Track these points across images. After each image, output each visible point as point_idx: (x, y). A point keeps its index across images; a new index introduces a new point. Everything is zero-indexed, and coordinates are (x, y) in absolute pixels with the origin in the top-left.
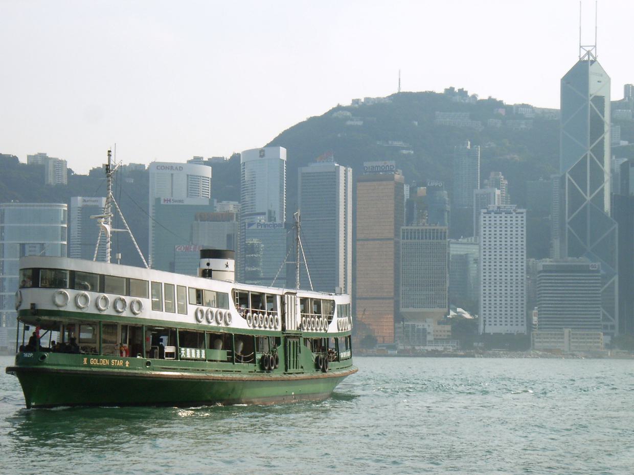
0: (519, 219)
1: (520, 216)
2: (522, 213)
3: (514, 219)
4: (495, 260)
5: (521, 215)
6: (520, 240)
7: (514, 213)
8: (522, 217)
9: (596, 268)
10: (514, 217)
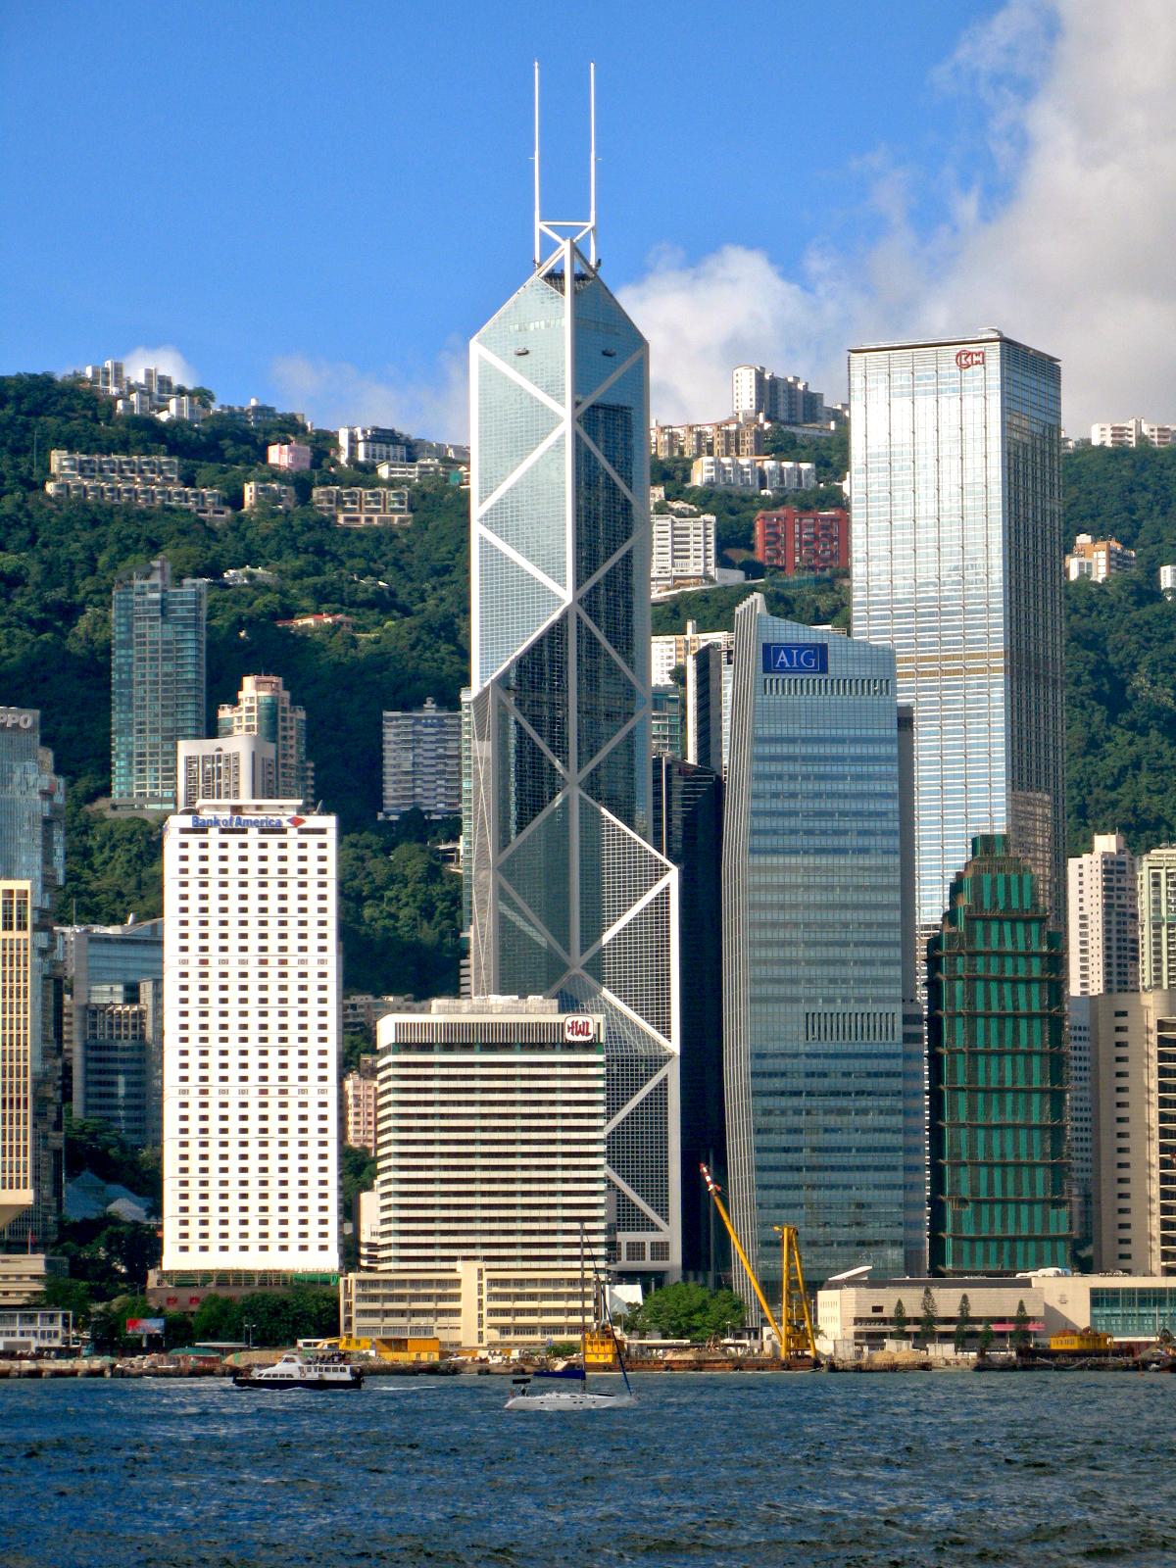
0: (312, 852)
1: (313, 840)
2: (322, 831)
3: (293, 852)
4: (283, 1007)
7: (293, 832)
8: (323, 846)
9: (588, 1034)
10: (293, 845)
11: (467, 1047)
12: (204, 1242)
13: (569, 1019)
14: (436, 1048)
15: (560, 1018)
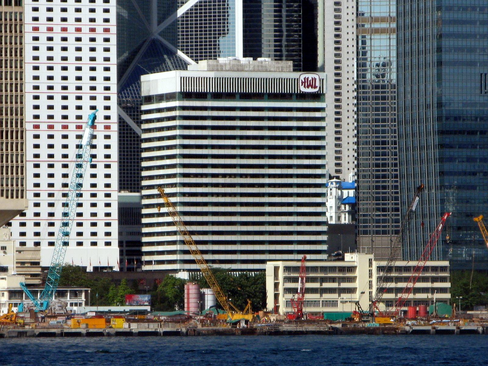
9: (315, 87)
11: (230, 96)
12: (94, 239)
13: (303, 76)
14: (209, 96)
15: (296, 75)
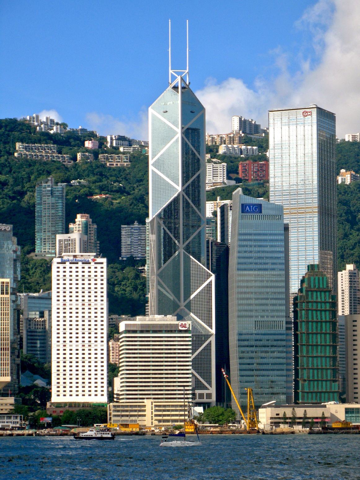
0: (99, 270)
1: (99, 266)
2: (102, 263)
5: (101, 265)
6: (99, 282)
7: (93, 263)
8: (102, 268)
9: (186, 327)
10: (93, 267)
11: (148, 332)
12: (64, 393)
13: (180, 323)
14: (138, 332)
15: (177, 322)
